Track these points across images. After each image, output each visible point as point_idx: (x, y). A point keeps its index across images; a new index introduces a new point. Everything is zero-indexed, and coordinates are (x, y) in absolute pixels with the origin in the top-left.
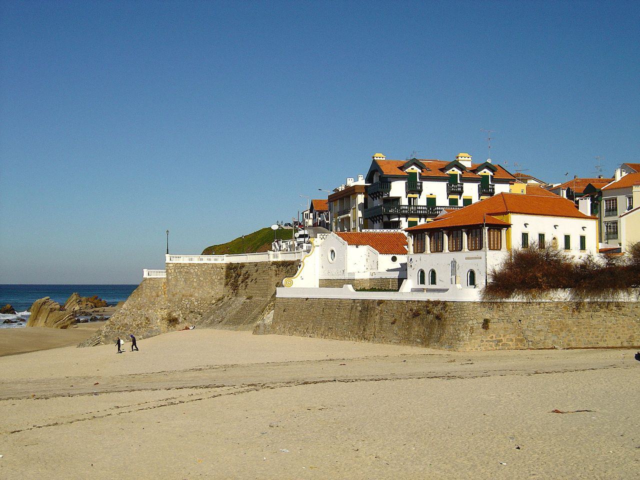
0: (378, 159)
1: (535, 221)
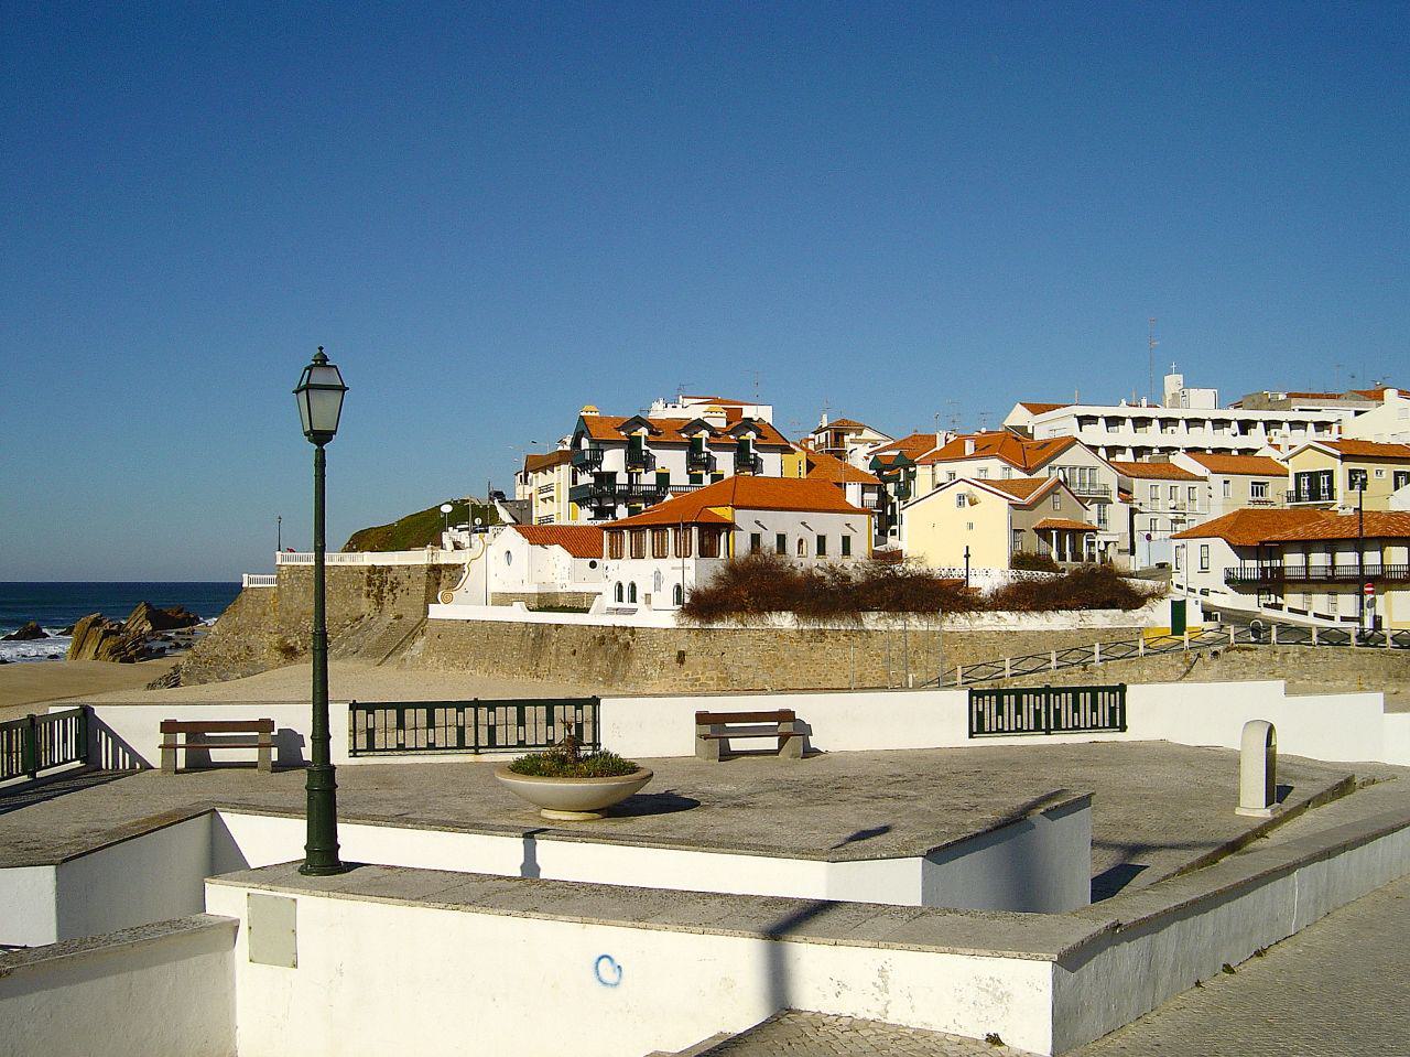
0: (589, 414)
1: (765, 516)
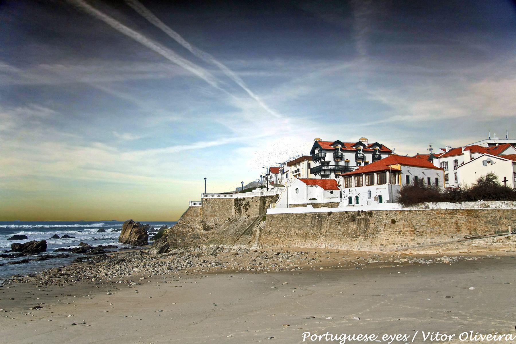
0: (319, 141)
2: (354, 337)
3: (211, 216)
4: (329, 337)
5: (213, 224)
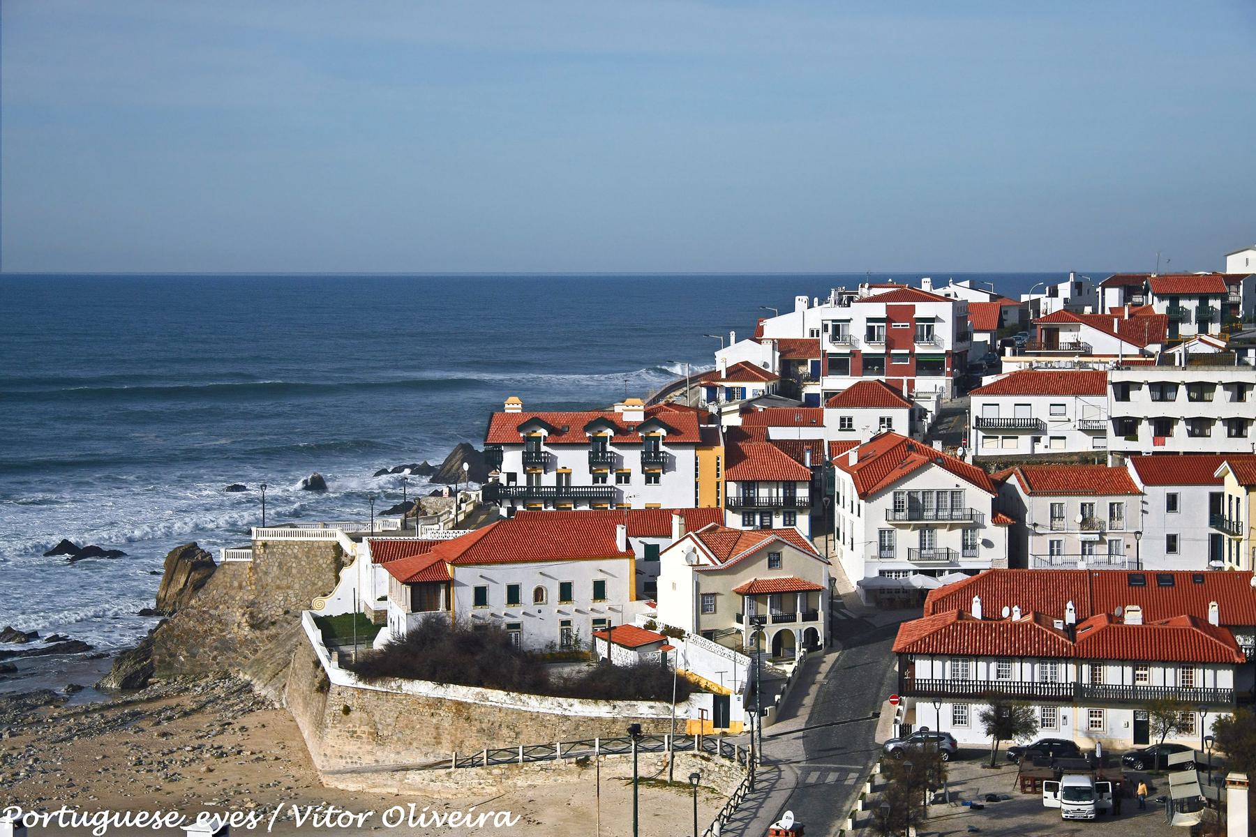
2: (127, 818)
3: (278, 587)
4: (67, 818)
5: (280, 610)
